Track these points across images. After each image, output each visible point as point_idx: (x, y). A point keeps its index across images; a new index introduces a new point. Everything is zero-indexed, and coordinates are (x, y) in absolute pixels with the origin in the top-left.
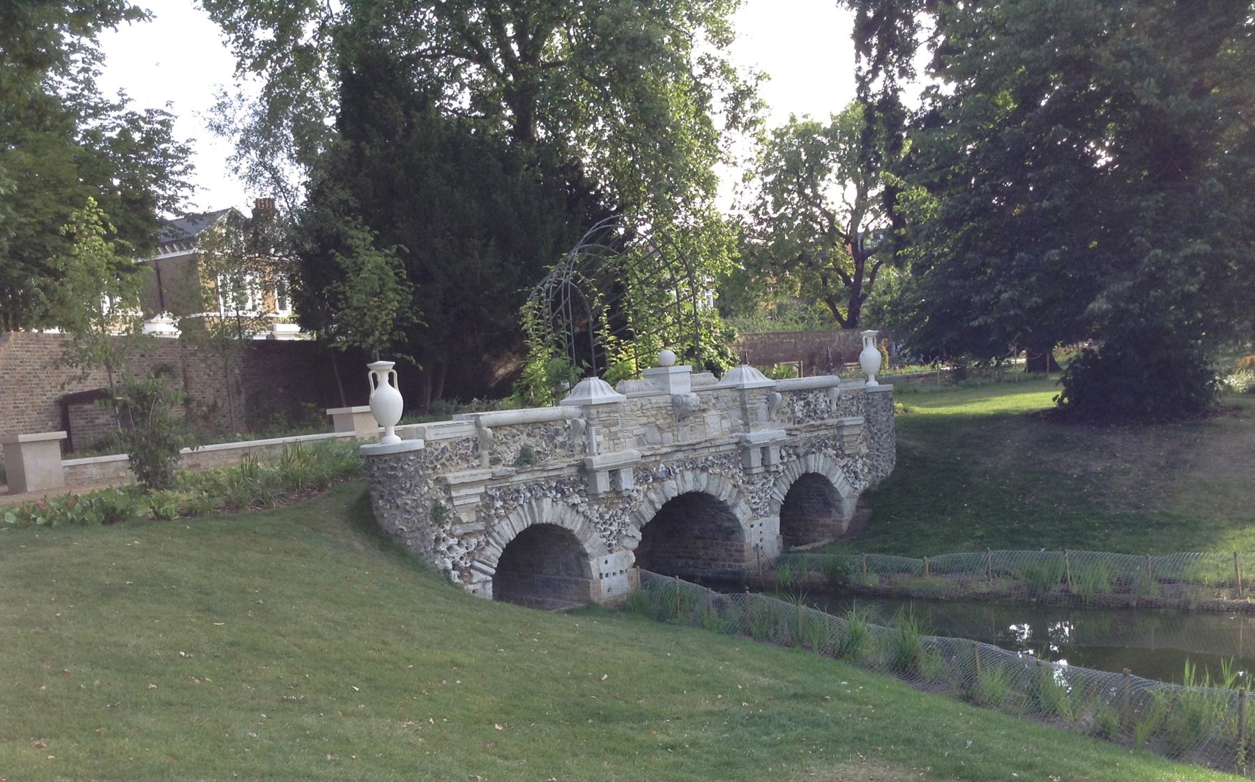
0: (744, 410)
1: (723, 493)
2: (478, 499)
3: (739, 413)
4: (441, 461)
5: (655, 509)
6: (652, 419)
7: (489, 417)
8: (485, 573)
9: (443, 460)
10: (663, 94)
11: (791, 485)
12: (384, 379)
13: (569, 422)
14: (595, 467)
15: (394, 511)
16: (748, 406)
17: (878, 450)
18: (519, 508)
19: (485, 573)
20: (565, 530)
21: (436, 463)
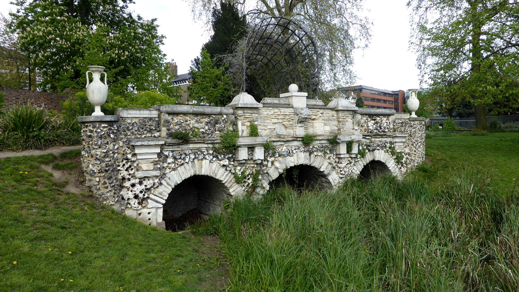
2: (156, 156)
9: (133, 130)
11: (364, 166)
15: (90, 159)
17: (415, 152)
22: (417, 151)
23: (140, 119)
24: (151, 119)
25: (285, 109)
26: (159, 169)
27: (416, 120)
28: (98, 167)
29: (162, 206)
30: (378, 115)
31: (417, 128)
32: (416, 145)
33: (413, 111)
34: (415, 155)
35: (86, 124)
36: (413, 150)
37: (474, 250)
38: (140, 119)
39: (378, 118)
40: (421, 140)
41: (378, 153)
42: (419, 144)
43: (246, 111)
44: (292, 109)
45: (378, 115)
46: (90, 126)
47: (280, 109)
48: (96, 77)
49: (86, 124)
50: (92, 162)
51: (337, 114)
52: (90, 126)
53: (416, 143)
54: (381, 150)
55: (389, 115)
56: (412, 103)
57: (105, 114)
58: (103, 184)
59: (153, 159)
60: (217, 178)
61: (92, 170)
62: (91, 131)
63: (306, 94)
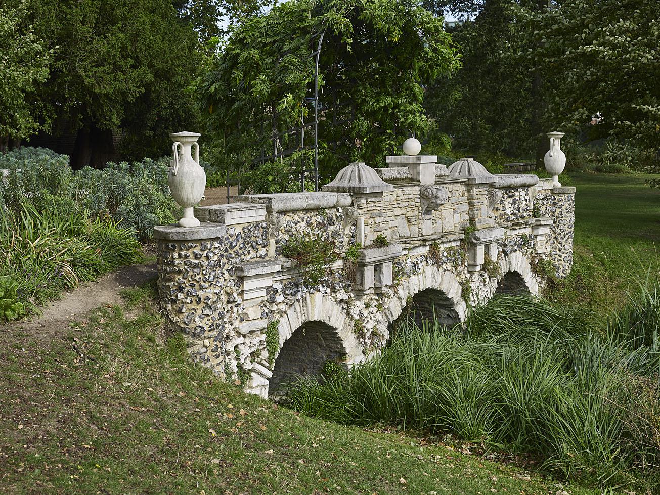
0: (471, 205)
1: (451, 291)
2: (264, 293)
3: (466, 207)
4: (235, 249)
5: (402, 306)
6: (404, 211)
7: (280, 200)
8: (262, 375)
9: (237, 248)
10: (60, 194)
11: (286, 340)
12: (187, 150)
13: (341, 210)
14: (367, 261)
15: (194, 306)
16: (475, 201)
17: (560, 251)
18: (297, 303)
19: (262, 375)
20: (331, 328)
21: (230, 251)
22: (563, 250)
23: (243, 225)
24: (257, 225)
25: (409, 188)
26: (174, 342)
27: (564, 193)
28: (208, 320)
29: (267, 382)
30: (516, 188)
31: (564, 208)
32: (562, 238)
33: (555, 174)
34: (560, 256)
35: (190, 244)
36: (555, 248)
37: (650, 420)
38: (243, 225)
39: (517, 194)
40: (569, 230)
41: (514, 257)
42: (567, 236)
43: (369, 200)
44: (418, 188)
45: (516, 188)
46: (195, 246)
47: (404, 188)
48: (187, 150)
49: (190, 244)
50: (199, 312)
51: (469, 191)
52: (195, 246)
53: (563, 234)
54: (518, 251)
55: (525, 186)
56: (555, 160)
57: (202, 220)
58: (214, 351)
59: (261, 299)
60: (330, 324)
61: (200, 327)
62: (196, 256)
63: (435, 158)
